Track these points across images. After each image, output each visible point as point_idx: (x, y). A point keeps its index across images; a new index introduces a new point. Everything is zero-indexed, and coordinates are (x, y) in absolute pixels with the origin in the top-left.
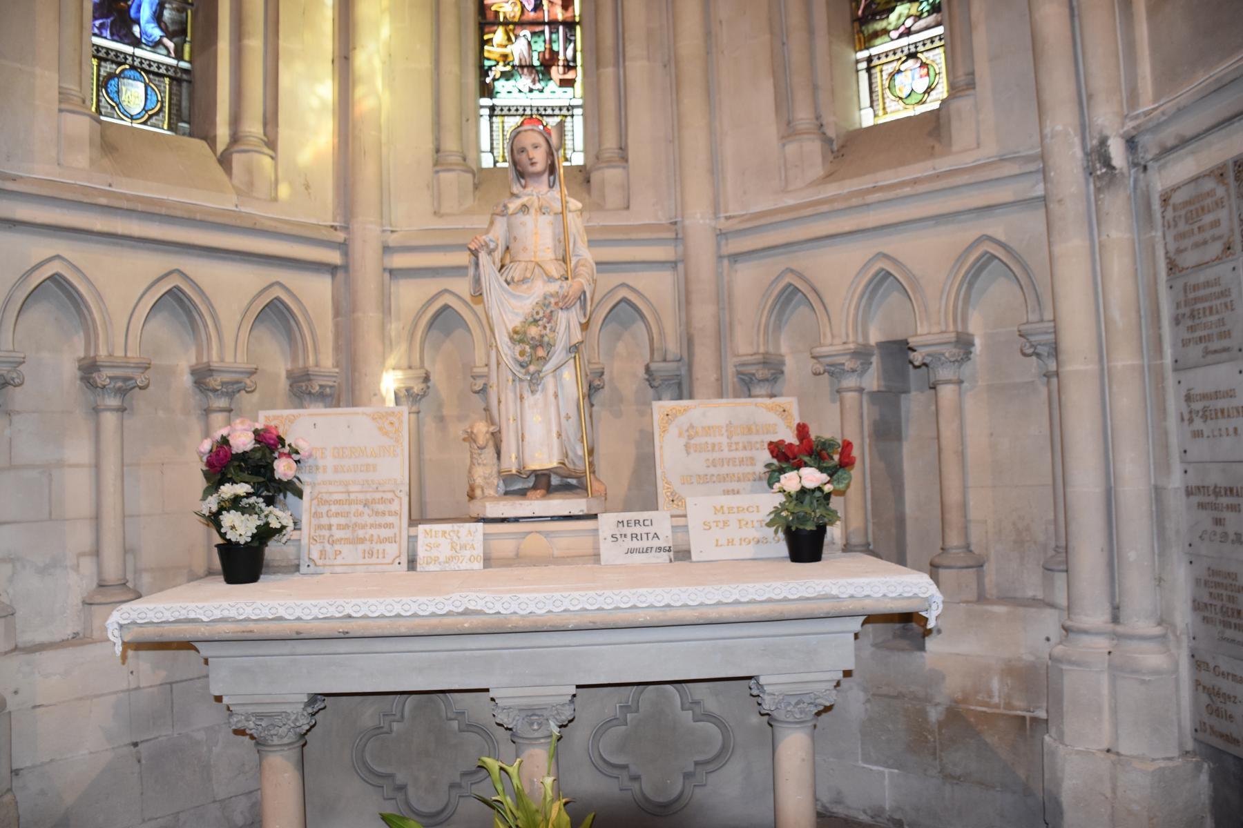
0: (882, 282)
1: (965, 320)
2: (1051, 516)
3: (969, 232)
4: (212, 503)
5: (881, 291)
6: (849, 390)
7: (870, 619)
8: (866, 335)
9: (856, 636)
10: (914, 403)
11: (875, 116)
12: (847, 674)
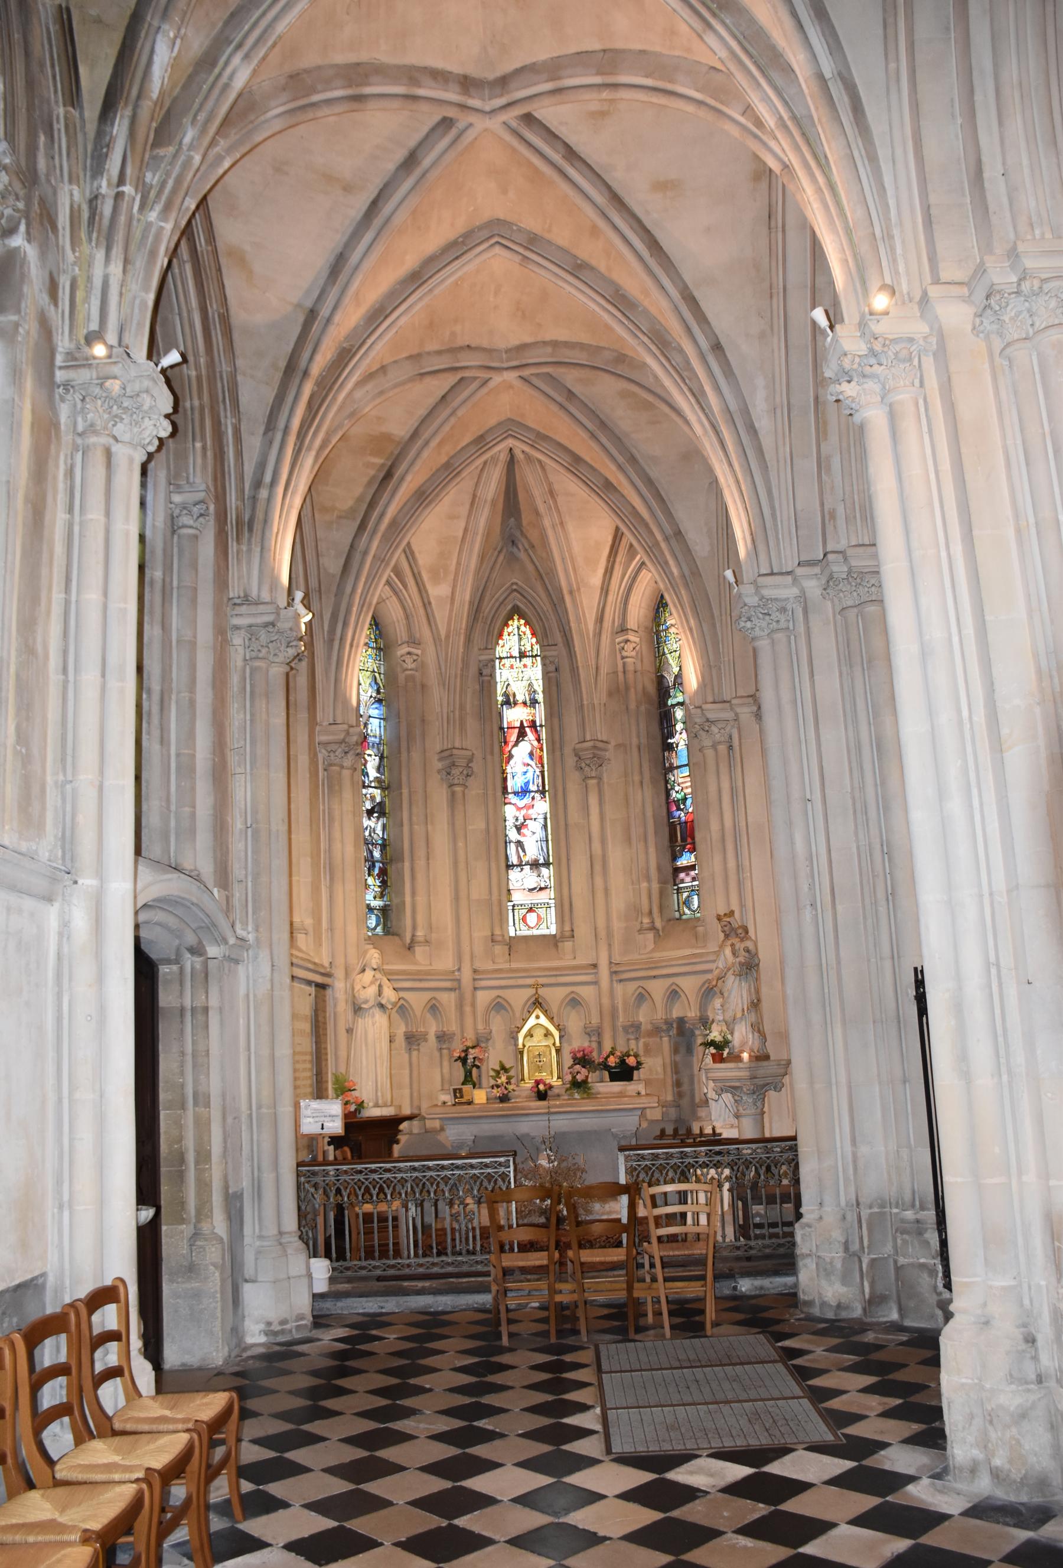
0: (674, 994)
1: (706, 1011)
4: (510, 1087)
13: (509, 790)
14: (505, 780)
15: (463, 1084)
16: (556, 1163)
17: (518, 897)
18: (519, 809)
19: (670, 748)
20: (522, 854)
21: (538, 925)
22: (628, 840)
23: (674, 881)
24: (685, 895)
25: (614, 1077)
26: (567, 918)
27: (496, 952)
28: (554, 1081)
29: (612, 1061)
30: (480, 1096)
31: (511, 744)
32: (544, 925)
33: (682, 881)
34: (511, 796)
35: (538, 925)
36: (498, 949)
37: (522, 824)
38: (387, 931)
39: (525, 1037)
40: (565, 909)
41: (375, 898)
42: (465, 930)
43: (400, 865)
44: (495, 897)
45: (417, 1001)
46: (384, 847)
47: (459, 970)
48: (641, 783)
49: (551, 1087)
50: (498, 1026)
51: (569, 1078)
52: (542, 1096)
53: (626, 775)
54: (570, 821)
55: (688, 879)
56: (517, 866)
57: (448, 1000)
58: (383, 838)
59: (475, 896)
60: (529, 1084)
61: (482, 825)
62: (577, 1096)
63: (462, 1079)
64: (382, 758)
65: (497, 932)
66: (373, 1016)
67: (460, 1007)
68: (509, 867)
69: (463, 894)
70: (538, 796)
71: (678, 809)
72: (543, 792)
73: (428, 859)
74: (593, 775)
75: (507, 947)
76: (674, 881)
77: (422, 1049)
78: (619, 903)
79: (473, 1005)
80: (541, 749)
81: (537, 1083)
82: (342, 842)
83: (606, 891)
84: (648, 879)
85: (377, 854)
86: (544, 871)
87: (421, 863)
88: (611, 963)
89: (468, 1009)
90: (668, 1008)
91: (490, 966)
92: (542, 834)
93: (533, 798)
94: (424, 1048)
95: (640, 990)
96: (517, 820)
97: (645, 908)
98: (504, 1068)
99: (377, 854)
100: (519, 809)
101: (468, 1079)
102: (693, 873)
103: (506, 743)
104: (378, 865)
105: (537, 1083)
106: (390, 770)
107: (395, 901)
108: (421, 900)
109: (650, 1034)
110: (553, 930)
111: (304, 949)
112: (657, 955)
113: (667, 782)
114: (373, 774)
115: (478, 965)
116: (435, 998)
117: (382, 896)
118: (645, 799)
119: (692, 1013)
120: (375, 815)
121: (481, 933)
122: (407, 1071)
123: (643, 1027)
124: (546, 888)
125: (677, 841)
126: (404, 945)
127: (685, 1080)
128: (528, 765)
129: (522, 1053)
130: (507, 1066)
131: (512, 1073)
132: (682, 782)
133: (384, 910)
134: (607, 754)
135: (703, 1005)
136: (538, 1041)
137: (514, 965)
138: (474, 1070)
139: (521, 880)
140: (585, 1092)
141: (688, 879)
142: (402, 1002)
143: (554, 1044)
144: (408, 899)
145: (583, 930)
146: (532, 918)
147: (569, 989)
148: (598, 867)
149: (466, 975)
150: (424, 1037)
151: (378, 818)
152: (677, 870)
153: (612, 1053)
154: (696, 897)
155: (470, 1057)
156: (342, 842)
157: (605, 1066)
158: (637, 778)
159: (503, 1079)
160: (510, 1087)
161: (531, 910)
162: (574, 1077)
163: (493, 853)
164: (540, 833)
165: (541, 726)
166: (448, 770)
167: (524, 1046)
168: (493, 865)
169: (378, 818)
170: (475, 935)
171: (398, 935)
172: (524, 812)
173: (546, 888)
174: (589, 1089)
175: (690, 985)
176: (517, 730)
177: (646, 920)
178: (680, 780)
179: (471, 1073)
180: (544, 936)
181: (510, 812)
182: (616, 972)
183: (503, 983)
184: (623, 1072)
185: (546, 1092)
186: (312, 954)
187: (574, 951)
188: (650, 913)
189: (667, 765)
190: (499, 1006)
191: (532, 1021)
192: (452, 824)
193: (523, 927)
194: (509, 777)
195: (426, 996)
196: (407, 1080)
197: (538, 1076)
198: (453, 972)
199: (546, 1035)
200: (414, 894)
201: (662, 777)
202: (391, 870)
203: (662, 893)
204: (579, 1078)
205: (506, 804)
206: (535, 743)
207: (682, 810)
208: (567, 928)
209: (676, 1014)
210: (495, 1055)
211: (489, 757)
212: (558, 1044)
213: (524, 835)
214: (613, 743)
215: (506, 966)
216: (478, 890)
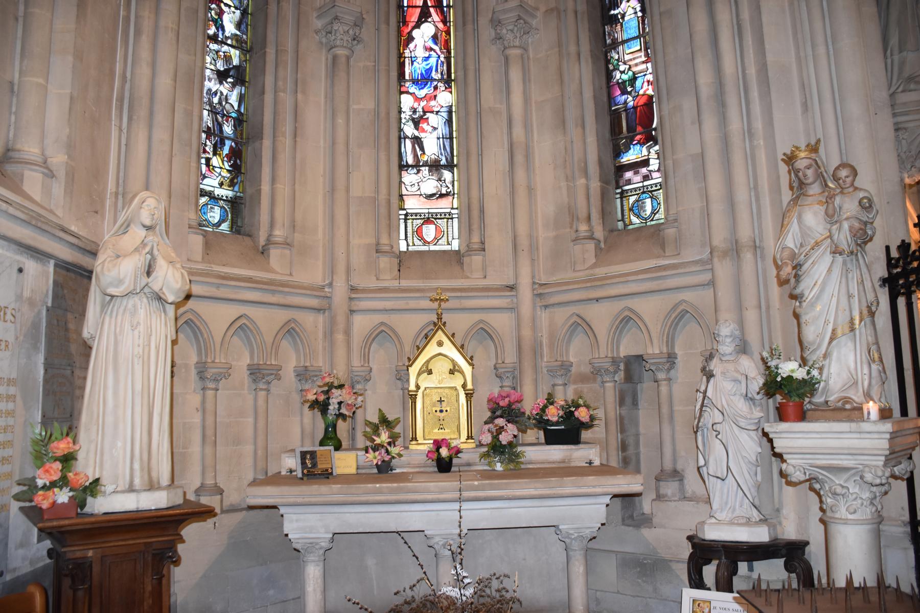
0: (626, 321)
1: (673, 347)
2: (897, 450)
3: (378, 318)
4: (394, 450)
5: (681, 323)
6: (261, 389)
7: (615, 496)
8: (618, 352)
9: (607, 505)
10: (645, 389)
11: (408, 245)
12: (603, 524)
13: (407, 77)
14: (402, 66)
15: (322, 444)
16: (469, 592)
17: (412, 204)
18: (417, 99)
19: (614, 20)
20: (419, 153)
21: (436, 240)
22: (562, 123)
23: (617, 182)
24: (632, 199)
25: (553, 438)
26: (475, 226)
27: (382, 265)
28: (461, 440)
29: (553, 414)
30: (345, 462)
31: (411, 25)
32: (444, 239)
33: (629, 182)
34: (407, 84)
35: (436, 240)
36: (385, 262)
37: (421, 117)
38: (236, 228)
39: (419, 374)
40: (473, 217)
41: (221, 184)
42: (341, 232)
43: (257, 144)
44: (383, 196)
45: (268, 321)
46: (239, 122)
47: (331, 285)
48: (579, 55)
49: (459, 451)
50: (381, 360)
51: (487, 439)
52: (444, 466)
53: (560, 45)
54: (485, 105)
55: (638, 178)
56: (413, 166)
57: (313, 323)
58: (238, 111)
59: (357, 190)
60: (423, 446)
61: (370, 105)
62: (499, 467)
63: (320, 434)
64: (244, 13)
65: (384, 240)
66: (134, 312)
67: (330, 334)
68: (403, 167)
69: (341, 184)
70: (441, 85)
71: (624, 92)
72: (448, 82)
73: (295, 136)
74: (517, 44)
75: (396, 261)
76: (617, 182)
77: (273, 389)
78: (547, 204)
79: (348, 333)
80: (448, 33)
81: (438, 444)
82: (153, 65)
83: (530, 190)
84: (585, 172)
85: (228, 129)
86: (447, 175)
87: (286, 142)
88: (534, 283)
89: (340, 337)
90: (616, 341)
91: (372, 283)
92: (446, 131)
93: (436, 88)
94: (276, 388)
95: (575, 318)
96: (415, 111)
97: (583, 213)
98: (385, 421)
99: (228, 129)
100: (417, 99)
101: (331, 438)
102: (644, 171)
103: (405, 23)
104: (228, 143)
105: (438, 444)
106: (254, 28)
107: (249, 191)
108: (283, 189)
109: (583, 379)
110: (455, 245)
111: (37, 197)
112: (601, 271)
113: (608, 62)
114: (230, 28)
115: (356, 281)
116: (295, 321)
117: (232, 184)
118: (584, 74)
119: (655, 349)
120: (230, 80)
121: (361, 239)
122: (251, 420)
123: (573, 369)
124: (447, 194)
125: (621, 132)
126: (256, 247)
127: (631, 441)
128: (431, 49)
129: (414, 398)
130: (391, 418)
131: (398, 429)
132: (631, 59)
133: (234, 203)
134: (534, 23)
135: (670, 341)
136: (439, 379)
137: (404, 283)
138: (341, 424)
139: (419, 186)
140: (511, 461)
141: (638, 178)
142: (243, 321)
143: (464, 386)
144: (265, 188)
145: (498, 242)
146: (429, 232)
147: (477, 317)
148: (519, 158)
149: (340, 292)
150: (276, 373)
151: (234, 85)
152: (621, 169)
153: (550, 400)
154: (648, 201)
155: (334, 402)
156: (153, 65)
157: (541, 422)
158: (573, 48)
159: (384, 437)
160: (394, 450)
161: (427, 221)
162: (496, 437)
163: (383, 141)
164: (442, 130)
165: (448, 6)
166: (329, 27)
167: (418, 387)
168: (383, 156)
169: (234, 85)
170: (355, 241)
171: (250, 236)
172: (423, 104)
173: (447, 194)
174: (518, 455)
175: (651, 309)
176: (419, 10)
177: (583, 227)
178: (627, 57)
179: (334, 426)
180: (444, 251)
181: (407, 102)
182: (540, 295)
183: (389, 305)
184: (568, 432)
185: (451, 459)
186: (59, 213)
187: (484, 268)
188: (589, 218)
189: (609, 41)
190: (383, 333)
191: (432, 349)
192: (331, 98)
193: (417, 242)
194: (407, 61)
195: (283, 315)
196: (249, 432)
197: (438, 434)
198: (323, 287)
199: (452, 372)
200: (273, 180)
201: (602, 57)
202: (248, 153)
203: (605, 197)
204: (504, 438)
205: (401, 93)
206: (441, 26)
207: (629, 93)
208: (476, 239)
209: (626, 349)
210: (376, 400)
211: (383, 27)
212: (469, 386)
213: (424, 131)
214: (543, 9)
215: (395, 283)
216: (361, 183)
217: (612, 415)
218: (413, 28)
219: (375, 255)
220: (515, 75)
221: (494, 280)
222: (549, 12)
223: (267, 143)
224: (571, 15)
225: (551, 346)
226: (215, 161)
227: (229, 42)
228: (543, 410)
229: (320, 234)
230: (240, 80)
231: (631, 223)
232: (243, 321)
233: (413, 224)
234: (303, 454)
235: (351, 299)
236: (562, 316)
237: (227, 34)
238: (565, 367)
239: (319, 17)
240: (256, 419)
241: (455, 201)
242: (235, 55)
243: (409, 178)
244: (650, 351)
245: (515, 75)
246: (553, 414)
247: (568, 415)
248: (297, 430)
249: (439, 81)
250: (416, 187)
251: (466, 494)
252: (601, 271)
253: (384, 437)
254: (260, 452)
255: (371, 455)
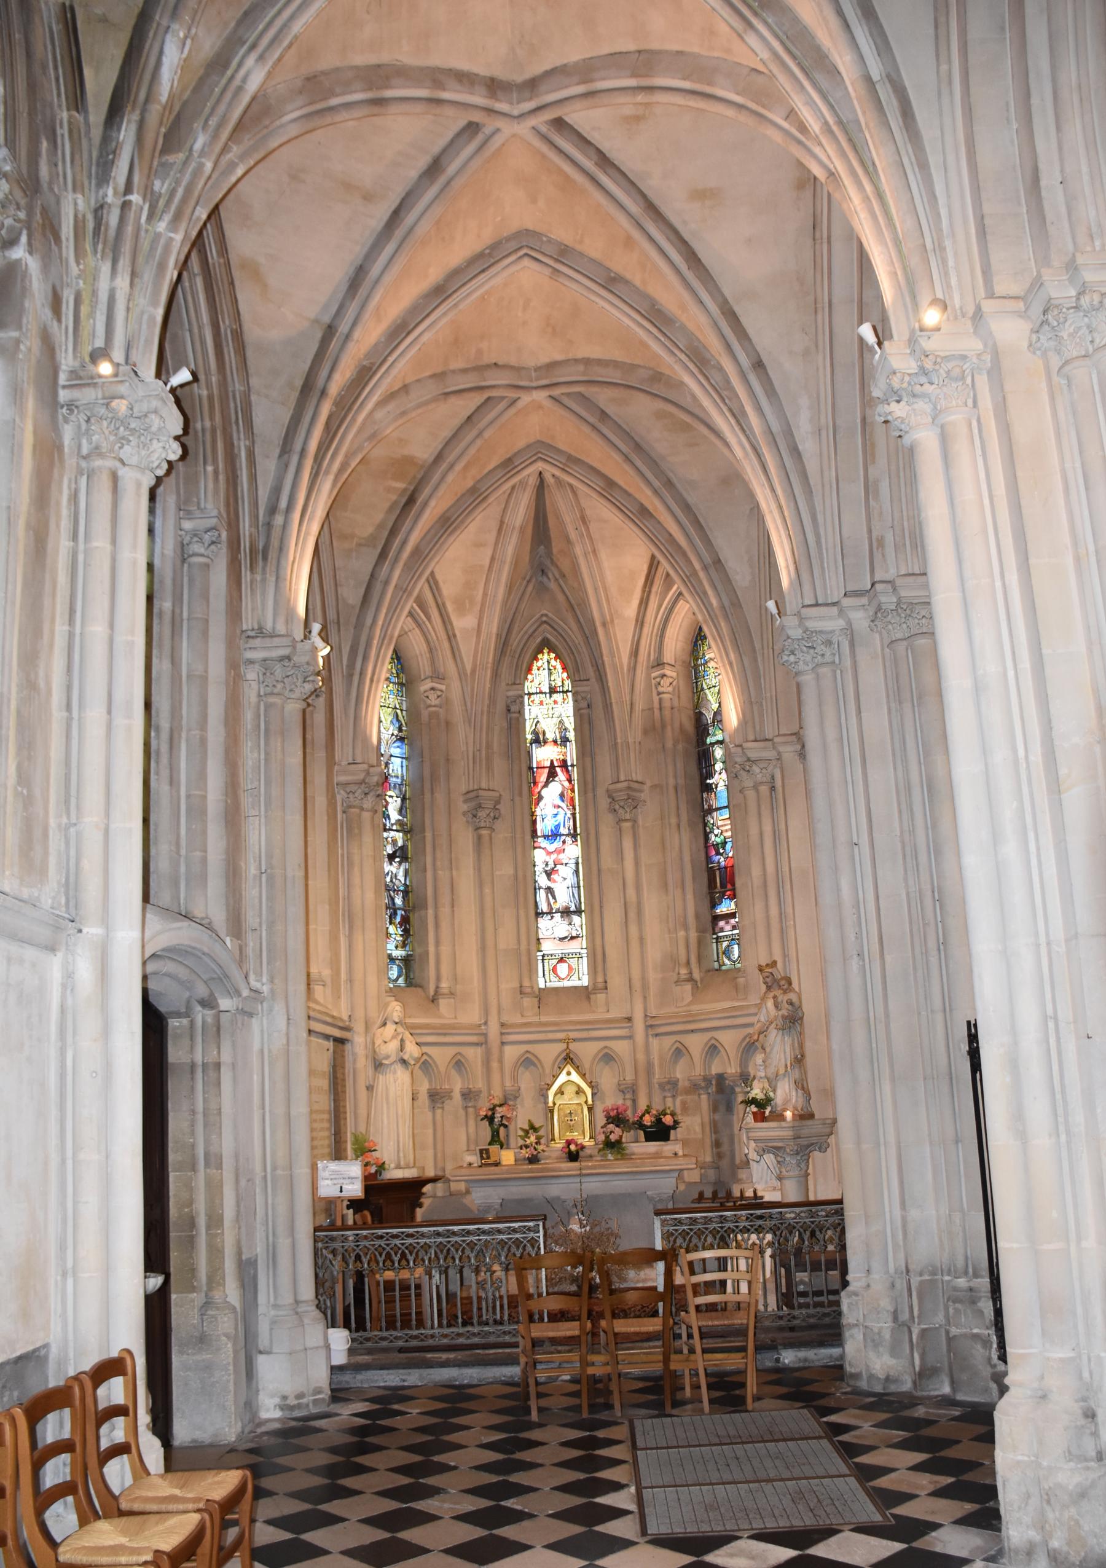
0: (713, 1049)
1: (747, 1066)
4: (540, 1148)
13: (539, 834)
16: (588, 1228)
17: (548, 947)
18: (549, 853)
19: (709, 789)
20: (552, 901)
21: (569, 976)
22: (665, 886)
23: (714, 929)
24: (725, 944)
25: (650, 1137)
27: (525, 1004)
28: (586, 1141)
29: (648, 1120)
30: (507, 1157)
31: (540, 785)
32: (576, 975)
33: (722, 930)
34: (540, 840)
35: (569, 976)
36: (527, 1002)
37: (553, 869)
38: (410, 983)
39: (556, 1094)
40: (597, 959)
41: (396, 947)
43: (423, 912)
44: (524, 946)
45: (442, 1056)
46: (406, 893)
47: (486, 1023)
48: (679, 826)
49: (583, 1147)
51: (602, 1138)
52: (573, 1157)
53: (662, 819)
55: (728, 928)
57: (473, 1055)
58: (405, 884)
59: (502, 945)
60: (559, 1144)
62: (610, 1157)
63: (489, 1139)
64: (404, 799)
65: (526, 983)
66: (395, 1072)
68: (539, 914)
69: (490, 942)
70: (569, 840)
71: (718, 853)
72: (574, 836)
76: (714, 929)
77: (446, 1107)
78: (655, 953)
79: (501, 1061)
80: (573, 791)
81: (569, 1143)
83: (642, 940)
84: (686, 928)
85: (399, 901)
86: (576, 919)
87: (445, 911)
88: (646, 1016)
89: (495, 1065)
91: (519, 1020)
93: (564, 842)
94: (448, 1105)
96: (547, 865)
98: (533, 1128)
99: (399, 901)
100: (549, 853)
101: (495, 1139)
102: (733, 921)
103: (535, 783)
104: (399, 912)
105: (569, 1143)
106: (413, 812)
107: (418, 951)
108: (445, 949)
109: (687, 1091)
110: (585, 981)
111: (322, 1001)
112: (695, 1008)
113: (705, 825)
114: (394, 816)
115: (505, 1018)
116: (459, 1053)
117: (404, 945)
118: (683, 842)
119: (732, 1070)
120: (397, 860)
121: (508, 984)
122: (430, 1131)
123: (680, 1084)
124: (577, 937)
125: (716, 887)
127: (725, 1140)
128: (559, 807)
129: (552, 1111)
130: (537, 1125)
131: (541, 1133)
132: (721, 824)
133: (407, 961)
135: (744, 1061)
136: (569, 1099)
137: (544, 1019)
139: (551, 928)
140: (619, 1153)
141: (728, 928)
142: (425, 1057)
143: (586, 1102)
144: (432, 949)
145: (616, 981)
146: (563, 969)
147: (602, 1044)
148: (632, 915)
149: (493, 1029)
150: (448, 1095)
151: (400, 863)
152: (716, 918)
153: (647, 1112)
154: (736, 947)
155: (498, 1115)
157: (640, 1125)
158: (674, 821)
159: (533, 1139)
160: (540, 1148)
161: (561, 960)
162: (607, 1137)
163: (521, 899)
164: (571, 880)
165: (572, 766)
167: (554, 1104)
168: (522, 912)
169: (400, 863)
170: (503, 986)
171: (421, 986)
172: (554, 856)
173: (577, 937)
175: (729, 1040)
176: (547, 770)
177: (684, 971)
178: (720, 823)
179: (498, 1133)
181: (539, 856)
182: (651, 1026)
184: (659, 1132)
185: (577, 1152)
186: (330, 1007)
187: (607, 1004)
188: (688, 963)
190: (528, 1061)
191: (562, 1078)
192: (478, 869)
194: (539, 819)
195: (451, 1051)
197: (569, 1136)
198: (480, 1026)
199: (577, 1093)
200: (437, 943)
201: (701, 820)
202: (414, 918)
204: (613, 1138)
205: (535, 848)
206: (566, 784)
207: (721, 854)
208: (600, 979)
209: (715, 1069)
210: (523, 1114)
211: (517, 799)
212: (590, 1102)
213: (555, 881)
214: (649, 783)
215: (536, 1019)
216: (506, 938)
217: (706, 1120)
218: (543, 787)
219: (519, 996)
220: (628, 844)
221: (615, 1013)
222: (654, 787)
223: (430, 912)
224: (672, 791)
225: (661, 1066)
226: (392, 929)
227: (394, 828)
228: (641, 1118)
229: (476, 984)
230: (404, 858)
231: (724, 964)
232: (425, 1057)
233: (550, 963)
234: (481, 1151)
235: (502, 1034)
236: (668, 1041)
237: (393, 821)
238: (673, 1083)
239: (465, 801)
240: (435, 1130)
241: (584, 941)
242: (399, 836)
243: (544, 923)
244: (729, 1071)
245: (628, 844)
246: (648, 1120)
247: (659, 1121)
248: (464, 1138)
249: (567, 835)
250: (550, 932)
251: (584, 1172)
252: (695, 1008)
253: (533, 1139)
254: (439, 1155)
255: (524, 1151)
